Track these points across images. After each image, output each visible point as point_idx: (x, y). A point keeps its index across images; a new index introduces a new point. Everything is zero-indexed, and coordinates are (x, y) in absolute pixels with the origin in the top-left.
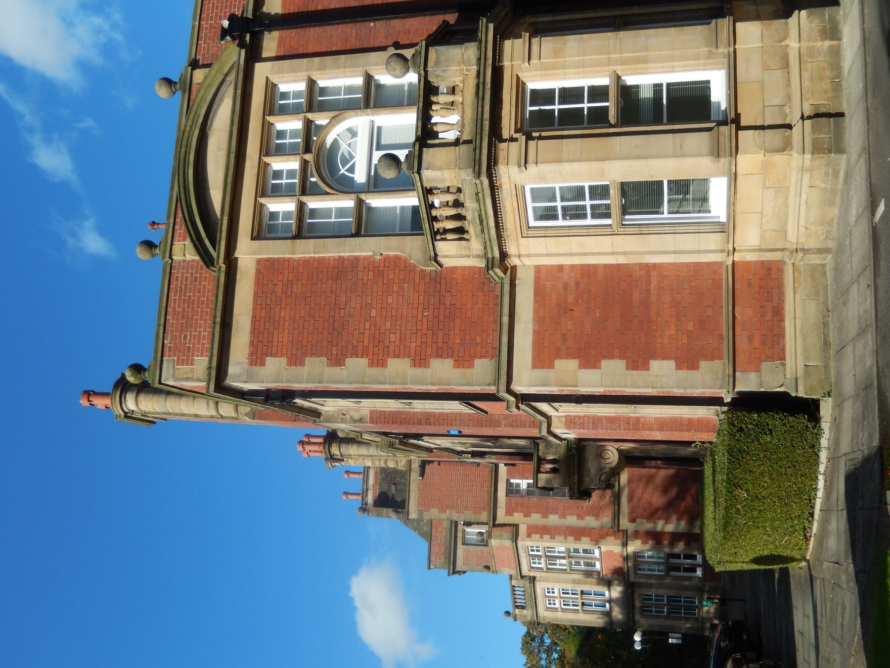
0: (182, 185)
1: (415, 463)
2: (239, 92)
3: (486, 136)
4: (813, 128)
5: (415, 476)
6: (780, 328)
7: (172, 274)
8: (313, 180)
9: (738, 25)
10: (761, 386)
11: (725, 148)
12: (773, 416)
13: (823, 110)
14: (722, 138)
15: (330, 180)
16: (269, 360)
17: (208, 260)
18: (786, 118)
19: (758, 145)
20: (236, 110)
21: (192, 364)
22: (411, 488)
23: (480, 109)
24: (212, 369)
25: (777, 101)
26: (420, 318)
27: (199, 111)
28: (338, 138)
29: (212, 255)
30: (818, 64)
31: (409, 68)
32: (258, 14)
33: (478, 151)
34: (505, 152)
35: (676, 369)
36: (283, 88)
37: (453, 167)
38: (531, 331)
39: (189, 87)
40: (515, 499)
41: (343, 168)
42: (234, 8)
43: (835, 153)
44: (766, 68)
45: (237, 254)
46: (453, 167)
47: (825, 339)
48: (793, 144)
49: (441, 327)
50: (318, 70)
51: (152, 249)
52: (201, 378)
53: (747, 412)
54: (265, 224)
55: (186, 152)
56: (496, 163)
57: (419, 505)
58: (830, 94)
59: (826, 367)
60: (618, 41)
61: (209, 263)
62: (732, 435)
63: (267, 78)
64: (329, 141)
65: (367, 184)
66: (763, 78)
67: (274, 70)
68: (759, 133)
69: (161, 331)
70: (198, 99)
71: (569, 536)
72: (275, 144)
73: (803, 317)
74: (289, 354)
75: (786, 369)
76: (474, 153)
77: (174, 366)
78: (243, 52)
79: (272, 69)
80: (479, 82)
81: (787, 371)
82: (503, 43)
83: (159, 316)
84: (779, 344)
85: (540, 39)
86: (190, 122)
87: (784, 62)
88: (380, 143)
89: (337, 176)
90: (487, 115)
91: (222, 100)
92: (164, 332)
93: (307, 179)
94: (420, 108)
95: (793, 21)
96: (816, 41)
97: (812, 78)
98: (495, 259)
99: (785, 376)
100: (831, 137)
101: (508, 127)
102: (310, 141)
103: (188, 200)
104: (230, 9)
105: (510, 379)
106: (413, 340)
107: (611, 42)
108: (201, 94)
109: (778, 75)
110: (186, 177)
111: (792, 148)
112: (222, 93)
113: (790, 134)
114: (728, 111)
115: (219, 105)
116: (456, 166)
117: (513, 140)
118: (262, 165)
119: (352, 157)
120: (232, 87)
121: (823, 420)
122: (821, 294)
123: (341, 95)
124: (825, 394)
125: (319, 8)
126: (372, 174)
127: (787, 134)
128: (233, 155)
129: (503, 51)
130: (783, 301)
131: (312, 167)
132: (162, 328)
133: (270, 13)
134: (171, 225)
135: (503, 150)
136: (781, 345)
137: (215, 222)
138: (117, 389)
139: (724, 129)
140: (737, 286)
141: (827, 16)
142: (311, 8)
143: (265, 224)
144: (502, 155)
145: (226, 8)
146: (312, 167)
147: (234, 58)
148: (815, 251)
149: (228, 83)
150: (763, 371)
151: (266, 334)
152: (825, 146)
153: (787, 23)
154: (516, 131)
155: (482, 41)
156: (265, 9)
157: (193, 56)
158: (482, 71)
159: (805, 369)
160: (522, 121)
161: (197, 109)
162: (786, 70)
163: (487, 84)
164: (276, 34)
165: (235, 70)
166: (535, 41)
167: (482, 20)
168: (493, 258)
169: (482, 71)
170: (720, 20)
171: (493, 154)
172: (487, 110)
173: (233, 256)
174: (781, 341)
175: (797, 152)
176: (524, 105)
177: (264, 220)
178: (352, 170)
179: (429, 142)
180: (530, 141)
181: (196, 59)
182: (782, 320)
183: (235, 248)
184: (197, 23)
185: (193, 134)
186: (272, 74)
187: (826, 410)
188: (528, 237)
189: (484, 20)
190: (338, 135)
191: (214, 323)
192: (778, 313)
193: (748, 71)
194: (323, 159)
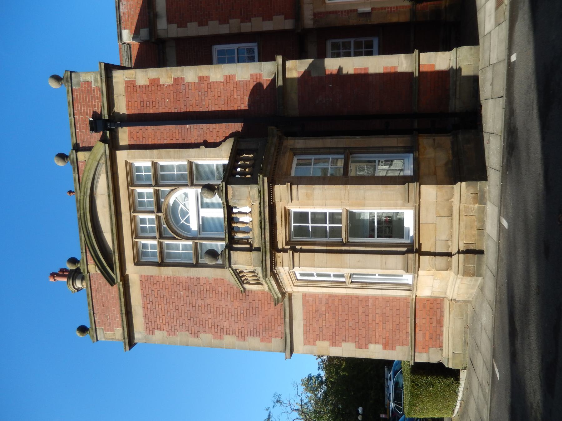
0: (86, 234)
2: (110, 174)
3: (268, 252)
4: (464, 260)
6: (440, 331)
7: (91, 280)
8: (165, 226)
9: (422, 186)
10: (429, 360)
11: (412, 268)
12: (434, 378)
13: (472, 248)
14: (410, 261)
15: (175, 226)
16: (157, 332)
17: (112, 281)
18: (449, 248)
19: (431, 266)
20: (110, 186)
21: (114, 331)
23: (263, 236)
24: (125, 339)
25: (444, 237)
26: (239, 314)
27: (86, 185)
28: (176, 200)
29: (113, 277)
30: (470, 218)
31: (216, 193)
32: (112, 114)
33: (264, 263)
34: (280, 259)
35: (383, 349)
36: (137, 164)
37: (250, 265)
38: (302, 325)
39: (76, 159)
41: (183, 220)
42: (95, 107)
43: (476, 276)
44: (438, 216)
45: (127, 273)
46: (250, 265)
47: (465, 340)
48: (452, 266)
49: (251, 319)
50: (157, 158)
51: (76, 264)
52: (120, 339)
53: (421, 376)
54: (140, 251)
55: (84, 213)
56: (275, 266)
58: (476, 238)
59: (464, 354)
60: (347, 192)
61: (112, 283)
62: (413, 387)
63: (126, 161)
64: (171, 202)
65: (199, 231)
66: (436, 222)
67: (129, 157)
68: (432, 258)
69: (92, 313)
70: (84, 179)
72: (138, 201)
73: (453, 328)
74: (168, 330)
75: (443, 352)
76: (262, 265)
77: (104, 332)
78: (107, 146)
79: (128, 156)
80: (261, 218)
81: (443, 353)
82: (274, 187)
83: (89, 305)
84: (439, 339)
85: (298, 186)
86: (82, 194)
87: (450, 212)
88: (203, 201)
89: (179, 224)
90: (268, 239)
91: (99, 175)
92: (94, 313)
93: (162, 226)
94: (226, 225)
95: (457, 187)
96: (471, 204)
97: (466, 227)
98: (279, 298)
99: (442, 356)
100: (475, 266)
101: (281, 243)
102: (160, 202)
103: (92, 243)
104: (93, 109)
105: (292, 350)
106: (237, 325)
107: (342, 192)
108: (86, 175)
109: (446, 220)
110: (87, 228)
111: (451, 269)
112: (99, 171)
113: (450, 260)
114: (414, 237)
115: (98, 178)
116: (252, 264)
117: (285, 251)
118: (133, 218)
119: (187, 213)
120: (104, 165)
121: (461, 380)
122: (464, 316)
123: (174, 172)
124: (463, 368)
125: (152, 111)
126: (201, 223)
127: (449, 260)
128: (113, 216)
129: (274, 193)
130: (443, 316)
131: (163, 220)
132: (92, 311)
133: (120, 113)
134: (85, 254)
135: (279, 257)
136: (441, 340)
137: (111, 253)
138: (70, 279)
139: (411, 256)
140: (417, 306)
141: (478, 188)
142: (147, 111)
143: (140, 251)
144: (279, 260)
145: (90, 107)
146: (163, 220)
147: (102, 150)
148: (462, 302)
149: (101, 165)
150: (430, 353)
151: (152, 318)
152: (471, 272)
153: (453, 188)
154: (287, 244)
155: (261, 191)
156: (116, 110)
157: (75, 141)
158: (262, 211)
159: (453, 354)
160: (289, 235)
161: (85, 185)
162: (451, 217)
163: (266, 219)
164: (126, 129)
165: (104, 156)
166: (294, 187)
167: (260, 176)
168: (278, 298)
169: (262, 211)
170: (411, 184)
171: (273, 261)
172: (267, 236)
173: (125, 274)
174: (441, 337)
175: (454, 272)
176: (290, 223)
177: (140, 250)
178: (188, 221)
179: (234, 246)
180: (293, 186)
181: (77, 143)
182: (442, 326)
183: (125, 270)
184: (72, 117)
185: (86, 200)
186: (128, 159)
187: (463, 375)
188: (297, 286)
189: (261, 176)
190: (176, 198)
191: (122, 314)
192: (440, 323)
193: (427, 217)
194: (170, 213)
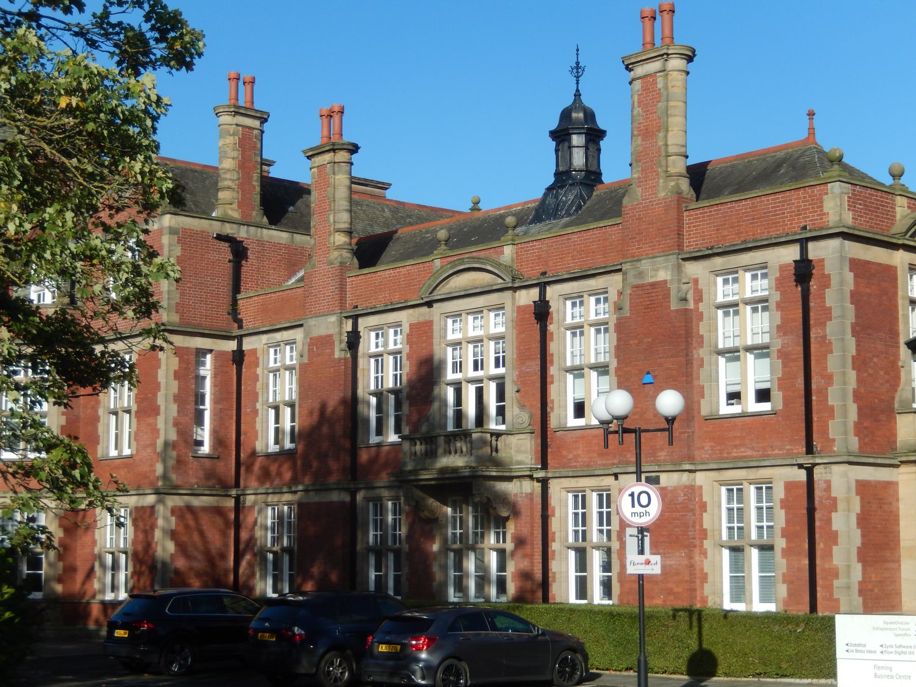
1: (231, 229)
5: (216, 228)
22: (203, 220)
40: (192, 358)
57: (185, 231)
71: (67, 418)
